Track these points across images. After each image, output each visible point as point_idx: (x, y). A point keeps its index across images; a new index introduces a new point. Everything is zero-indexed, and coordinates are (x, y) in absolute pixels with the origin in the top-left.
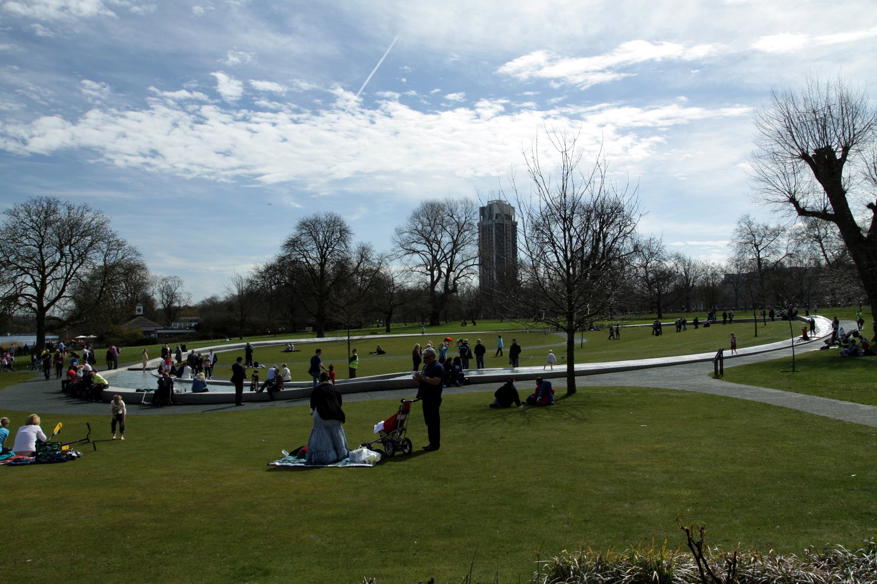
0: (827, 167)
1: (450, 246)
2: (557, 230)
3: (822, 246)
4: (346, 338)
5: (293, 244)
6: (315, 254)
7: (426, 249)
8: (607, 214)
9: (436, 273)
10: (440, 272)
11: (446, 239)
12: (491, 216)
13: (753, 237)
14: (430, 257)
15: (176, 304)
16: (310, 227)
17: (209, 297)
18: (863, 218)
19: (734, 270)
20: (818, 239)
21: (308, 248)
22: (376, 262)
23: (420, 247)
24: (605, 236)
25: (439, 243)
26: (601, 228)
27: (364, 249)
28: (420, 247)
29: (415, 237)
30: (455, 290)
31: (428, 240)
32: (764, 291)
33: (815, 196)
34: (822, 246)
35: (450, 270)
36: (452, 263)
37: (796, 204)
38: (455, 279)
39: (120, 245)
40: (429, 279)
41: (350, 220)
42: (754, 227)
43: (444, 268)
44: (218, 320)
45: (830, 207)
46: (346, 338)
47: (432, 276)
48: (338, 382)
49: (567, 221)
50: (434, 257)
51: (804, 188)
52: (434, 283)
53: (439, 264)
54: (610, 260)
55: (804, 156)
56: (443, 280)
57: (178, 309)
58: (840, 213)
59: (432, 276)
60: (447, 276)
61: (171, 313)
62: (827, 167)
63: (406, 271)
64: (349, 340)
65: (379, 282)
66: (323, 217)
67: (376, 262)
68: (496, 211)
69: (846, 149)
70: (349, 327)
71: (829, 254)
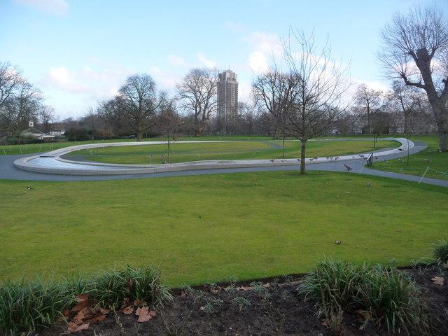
0: (423, 60)
1: (206, 95)
2: (267, 87)
3: (401, 102)
4: (167, 142)
5: (124, 90)
6: (136, 95)
7: (193, 95)
8: (296, 80)
9: (198, 109)
10: (200, 108)
11: (204, 90)
12: (224, 79)
13: (364, 97)
14: (195, 100)
15: (50, 122)
16: (134, 81)
17: (67, 118)
18: (439, 86)
19: (352, 113)
20: (400, 98)
21: (132, 92)
22: (169, 101)
23: (189, 94)
24: (292, 93)
25: (200, 92)
26: (290, 88)
27: (163, 94)
28: (189, 94)
29: (187, 89)
30: (208, 118)
31: (194, 90)
32: (376, 124)
33: (415, 75)
34: (401, 102)
35: (206, 107)
36: (207, 103)
37: (405, 79)
38: (209, 112)
39: (29, 86)
40: (194, 111)
41: (155, 79)
42: (367, 90)
43: (203, 106)
44: (77, 132)
45: (423, 81)
46: (167, 142)
47: (196, 110)
48: (283, 153)
49: (272, 82)
50: (197, 100)
51: (409, 71)
52: (197, 114)
53: (200, 104)
54: (291, 102)
55: (411, 53)
56: (202, 112)
57: (51, 125)
58: (429, 86)
59: (196, 110)
60: (204, 111)
61: (47, 127)
62: (423, 60)
63: (183, 108)
64: (169, 144)
65: (169, 113)
66: (140, 76)
67: (169, 101)
68: (228, 76)
69: (434, 50)
70: (168, 138)
71: (405, 106)
